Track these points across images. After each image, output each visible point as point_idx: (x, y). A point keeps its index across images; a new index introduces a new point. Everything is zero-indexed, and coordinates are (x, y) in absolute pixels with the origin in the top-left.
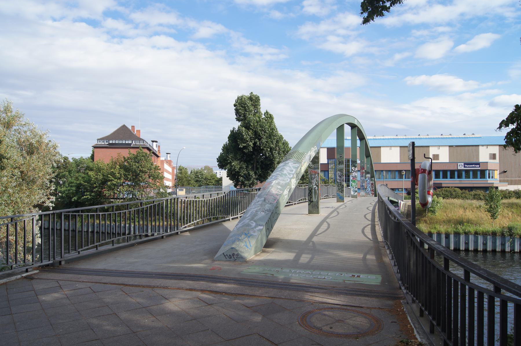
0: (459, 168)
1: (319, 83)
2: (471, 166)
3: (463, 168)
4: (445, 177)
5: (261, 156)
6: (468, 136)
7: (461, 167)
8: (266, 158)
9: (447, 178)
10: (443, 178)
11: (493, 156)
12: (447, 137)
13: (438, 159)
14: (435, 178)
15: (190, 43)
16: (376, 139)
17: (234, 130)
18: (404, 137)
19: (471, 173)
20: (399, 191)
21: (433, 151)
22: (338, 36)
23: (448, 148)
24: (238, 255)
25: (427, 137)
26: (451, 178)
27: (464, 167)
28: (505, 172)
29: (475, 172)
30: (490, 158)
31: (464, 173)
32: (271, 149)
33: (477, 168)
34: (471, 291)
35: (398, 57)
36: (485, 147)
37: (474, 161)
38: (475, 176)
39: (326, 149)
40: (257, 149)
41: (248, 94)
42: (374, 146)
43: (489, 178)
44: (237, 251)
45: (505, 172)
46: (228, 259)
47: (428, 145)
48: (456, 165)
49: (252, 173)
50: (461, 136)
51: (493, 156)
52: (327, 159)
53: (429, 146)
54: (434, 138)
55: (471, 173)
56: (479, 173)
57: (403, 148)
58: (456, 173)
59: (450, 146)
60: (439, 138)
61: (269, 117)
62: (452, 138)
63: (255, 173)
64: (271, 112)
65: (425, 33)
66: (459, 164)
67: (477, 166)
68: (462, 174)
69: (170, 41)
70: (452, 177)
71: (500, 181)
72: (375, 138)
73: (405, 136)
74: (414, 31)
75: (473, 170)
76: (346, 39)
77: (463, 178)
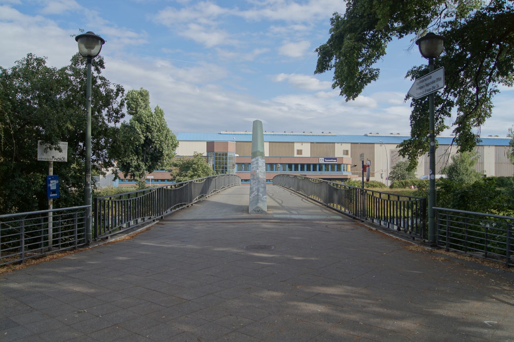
0: (320, 162)
1: (181, 73)
2: (330, 160)
3: (323, 162)
4: (309, 169)
5: (150, 148)
6: (326, 134)
7: (322, 161)
8: (155, 149)
9: (310, 171)
10: (307, 170)
11: (346, 152)
12: (309, 134)
13: (301, 154)
14: (331, 171)
15: (39, 18)
16: (247, 134)
17: (124, 123)
18: (272, 133)
19: (330, 167)
20: (270, 182)
21: (297, 146)
22: (199, 24)
23: (309, 144)
24: (262, 210)
25: (292, 134)
26: (313, 170)
27: (325, 161)
28: (356, 166)
29: (333, 166)
30: (344, 154)
31: (324, 166)
32: (161, 141)
33: (335, 162)
34: (400, 202)
35: (257, 52)
36: (340, 144)
37: (331, 157)
38: (333, 169)
39: (205, 143)
40: (148, 142)
41: (138, 89)
42: (243, 141)
43: (344, 170)
44: (261, 208)
45: (356, 166)
46: (257, 213)
47: (293, 141)
48: (318, 160)
49: (142, 164)
50: (320, 134)
51: (346, 152)
52: (207, 152)
53: (293, 143)
54: (297, 135)
55: (330, 167)
56: (336, 167)
57: (271, 143)
58: (318, 166)
59: (311, 143)
60: (301, 135)
61: (159, 113)
62: (313, 135)
63: (146, 165)
64: (161, 107)
65: (282, 30)
66: (320, 159)
67: (334, 160)
68: (322, 167)
69: (15, 14)
70: (314, 169)
71: (353, 174)
72: (246, 133)
73: (273, 132)
74: (272, 27)
75: (331, 164)
76: (207, 28)
77: (287, 170)
